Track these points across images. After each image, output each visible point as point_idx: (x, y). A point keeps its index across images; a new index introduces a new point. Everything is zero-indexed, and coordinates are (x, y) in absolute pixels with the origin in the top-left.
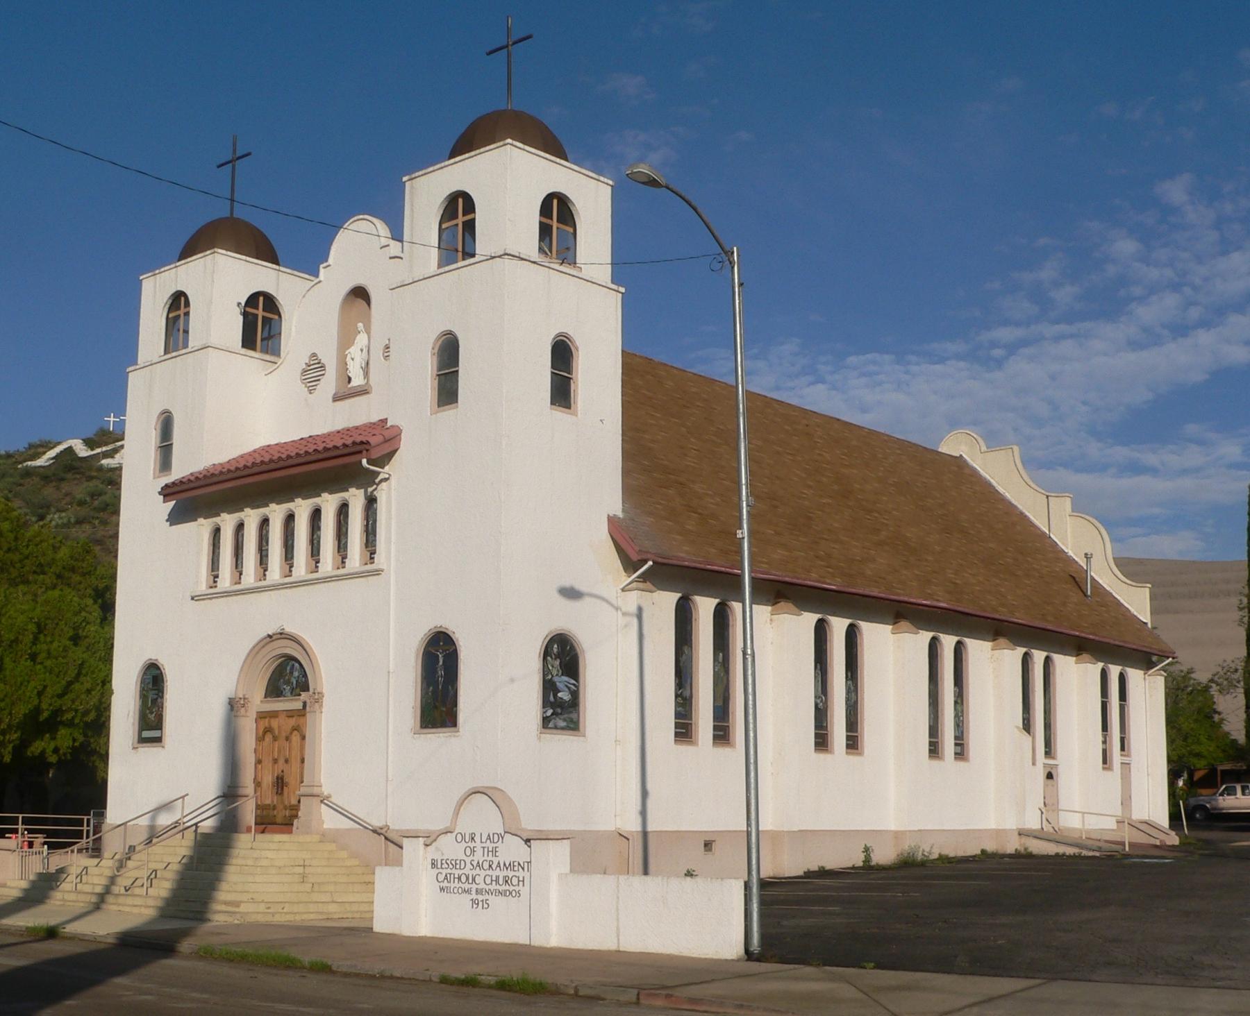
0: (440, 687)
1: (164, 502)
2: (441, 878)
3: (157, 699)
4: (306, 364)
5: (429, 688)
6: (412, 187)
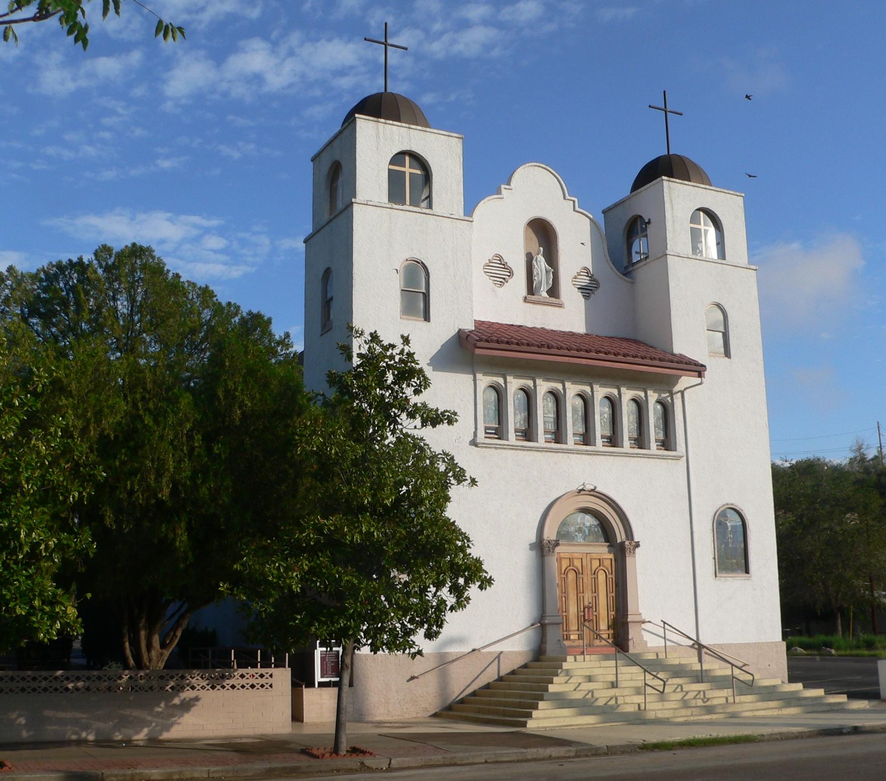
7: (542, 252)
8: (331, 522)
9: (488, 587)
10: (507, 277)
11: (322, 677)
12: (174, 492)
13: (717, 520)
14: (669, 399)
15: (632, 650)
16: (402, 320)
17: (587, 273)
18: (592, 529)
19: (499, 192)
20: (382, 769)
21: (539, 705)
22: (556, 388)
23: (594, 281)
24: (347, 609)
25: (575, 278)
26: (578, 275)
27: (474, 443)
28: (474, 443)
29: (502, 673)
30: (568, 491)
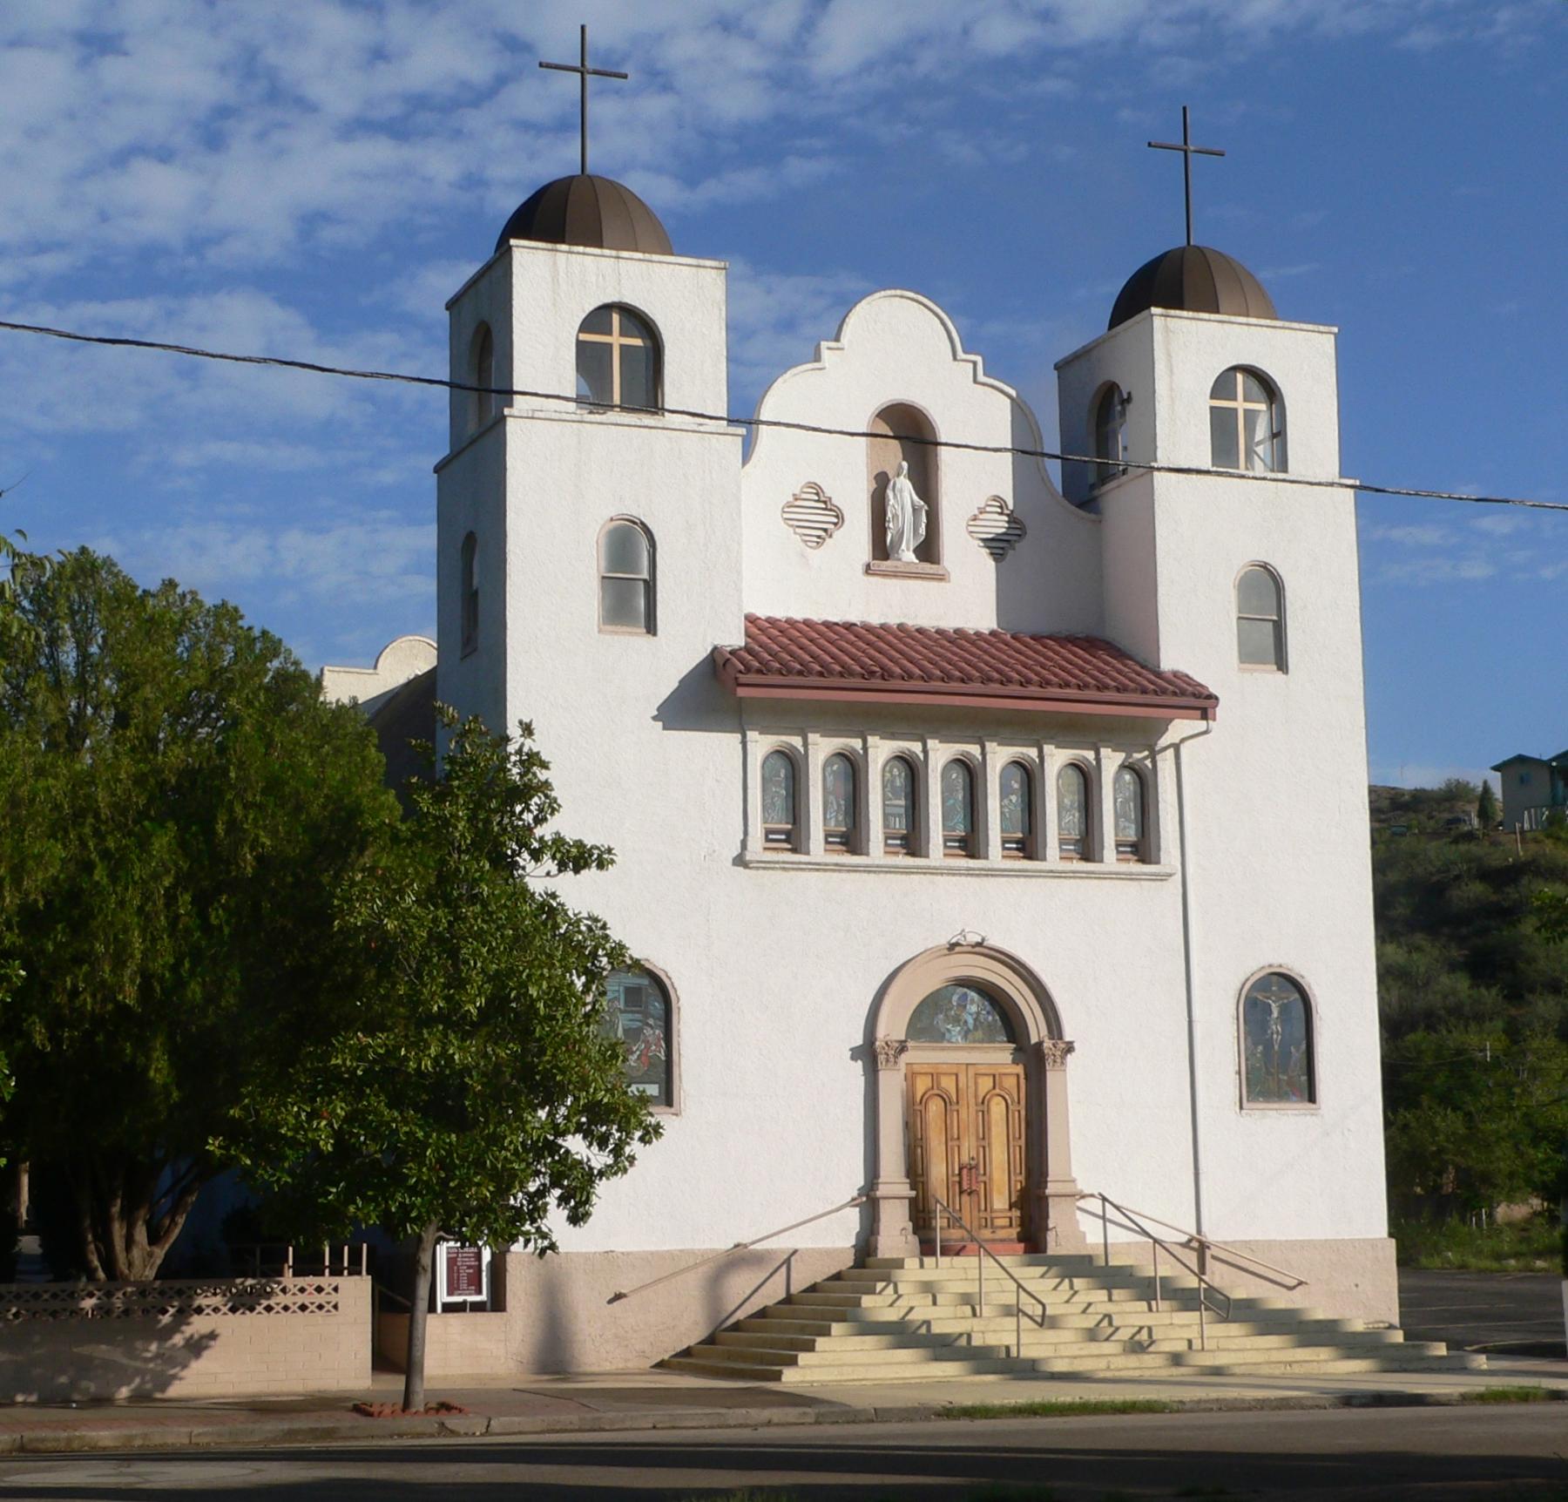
4: (794, 495)
5: (1256, 1048)
6: (1166, 329)
7: (905, 471)
8: (379, 1040)
9: (654, 1140)
10: (832, 526)
11: (450, 1293)
12: (145, 990)
13: (1246, 997)
14: (1148, 763)
15: (1053, 1249)
16: (602, 636)
17: (1001, 507)
18: (982, 1018)
19: (817, 357)
20: (474, 1434)
21: (817, 1344)
22: (909, 750)
23: (1015, 523)
24: (407, 1177)
25: (974, 520)
26: (981, 513)
27: (740, 861)
28: (740, 861)
29: (794, 1290)
30: (930, 946)
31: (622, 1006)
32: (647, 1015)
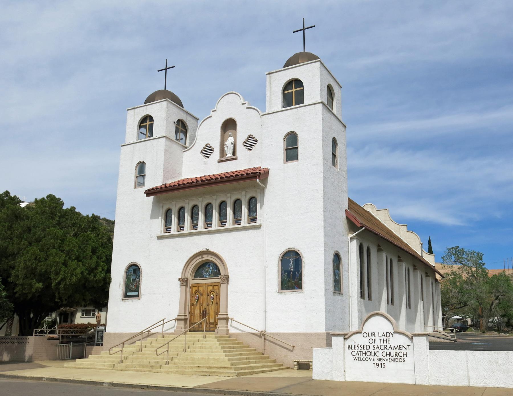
0: (291, 273)
1: (146, 197)
2: (354, 353)
3: (135, 279)
26: (247, 140)
31: (132, 274)
32: (137, 275)
